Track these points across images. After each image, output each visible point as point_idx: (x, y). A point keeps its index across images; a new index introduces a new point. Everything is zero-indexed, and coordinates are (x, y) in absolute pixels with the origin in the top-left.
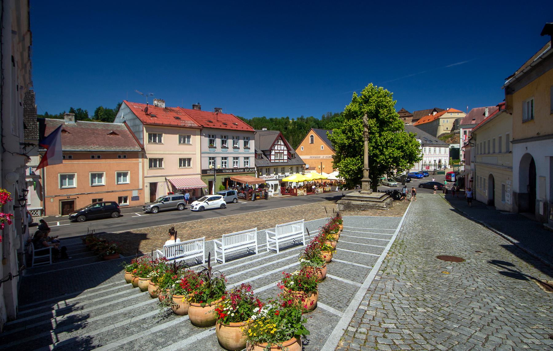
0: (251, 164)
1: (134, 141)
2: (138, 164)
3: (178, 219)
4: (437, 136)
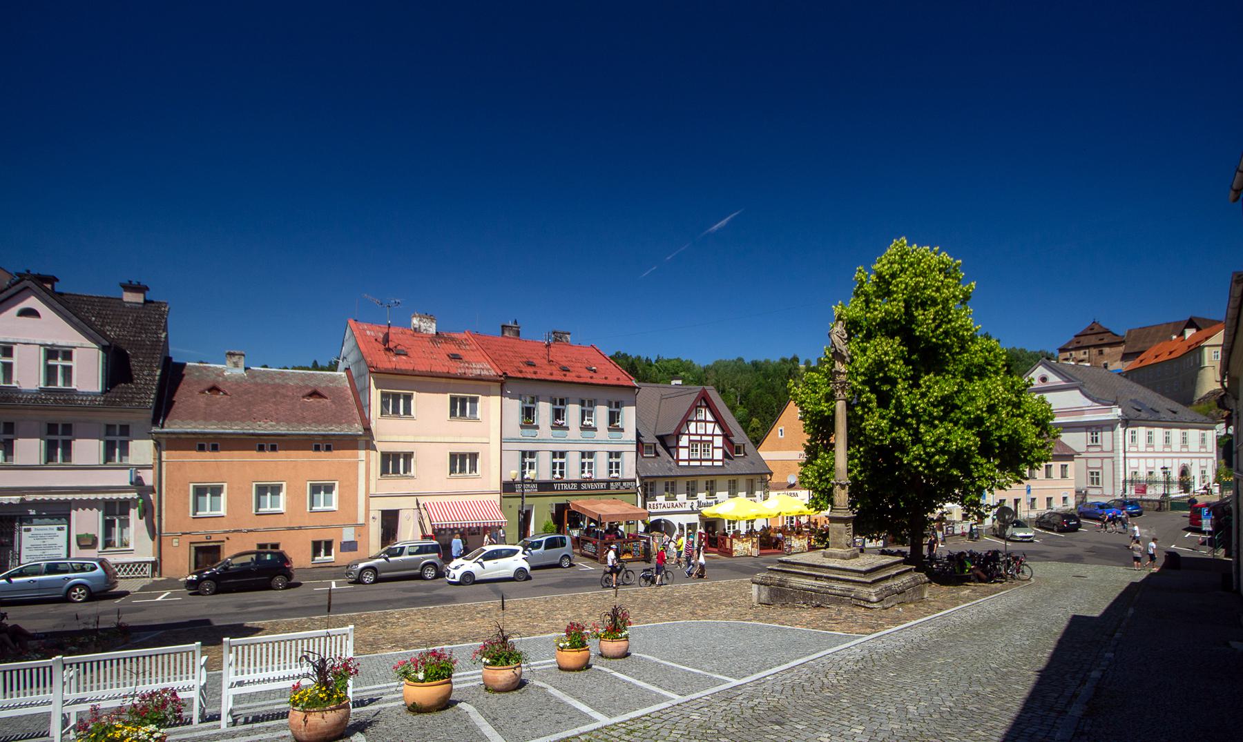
0: (626, 471)
1: (356, 411)
2: (355, 466)
3: (398, 600)
4: (1196, 399)
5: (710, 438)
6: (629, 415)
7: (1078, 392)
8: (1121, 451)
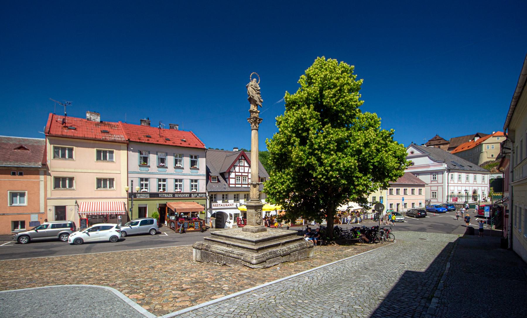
4: (479, 165)
5: (247, 174)
6: (202, 163)
7: (427, 157)
8: (446, 183)
